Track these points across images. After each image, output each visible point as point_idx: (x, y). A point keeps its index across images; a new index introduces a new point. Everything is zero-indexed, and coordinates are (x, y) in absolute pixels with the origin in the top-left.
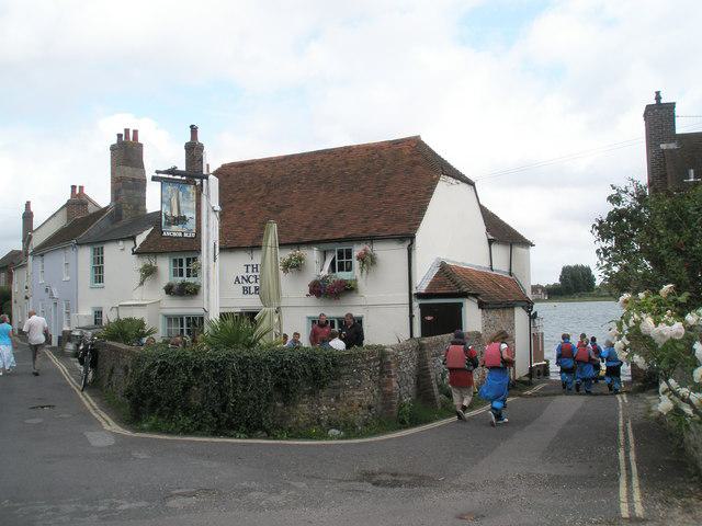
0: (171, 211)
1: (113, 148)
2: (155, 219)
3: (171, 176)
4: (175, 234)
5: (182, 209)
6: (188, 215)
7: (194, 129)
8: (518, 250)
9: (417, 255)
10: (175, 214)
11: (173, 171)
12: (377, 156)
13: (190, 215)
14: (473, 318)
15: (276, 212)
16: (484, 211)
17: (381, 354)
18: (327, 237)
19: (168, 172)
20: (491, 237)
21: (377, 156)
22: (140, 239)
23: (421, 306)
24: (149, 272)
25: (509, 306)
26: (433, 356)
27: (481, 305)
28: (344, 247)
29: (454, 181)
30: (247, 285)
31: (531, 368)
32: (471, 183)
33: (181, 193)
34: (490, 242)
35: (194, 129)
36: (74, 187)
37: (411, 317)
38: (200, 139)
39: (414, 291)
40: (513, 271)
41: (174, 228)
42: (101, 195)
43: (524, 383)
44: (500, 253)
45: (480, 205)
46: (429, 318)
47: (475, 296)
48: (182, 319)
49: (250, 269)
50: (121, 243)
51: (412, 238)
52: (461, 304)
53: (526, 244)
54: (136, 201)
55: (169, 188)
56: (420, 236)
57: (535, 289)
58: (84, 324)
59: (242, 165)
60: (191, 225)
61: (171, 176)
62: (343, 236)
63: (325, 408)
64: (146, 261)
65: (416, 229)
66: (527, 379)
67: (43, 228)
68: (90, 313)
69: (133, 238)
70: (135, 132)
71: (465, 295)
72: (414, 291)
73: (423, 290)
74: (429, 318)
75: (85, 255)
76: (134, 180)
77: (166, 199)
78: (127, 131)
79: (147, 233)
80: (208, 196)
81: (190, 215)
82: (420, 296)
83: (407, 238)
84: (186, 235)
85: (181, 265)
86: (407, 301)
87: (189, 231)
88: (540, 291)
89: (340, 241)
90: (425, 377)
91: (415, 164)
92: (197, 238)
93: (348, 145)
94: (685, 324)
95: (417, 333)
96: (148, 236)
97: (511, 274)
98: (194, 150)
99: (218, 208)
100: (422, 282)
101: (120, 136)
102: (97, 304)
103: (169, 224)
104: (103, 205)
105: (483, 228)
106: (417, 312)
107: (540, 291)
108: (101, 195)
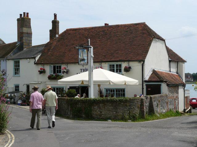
1: (18, 20)
7: (55, 16)
8: (180, 64)
10: (82, 58)
12: (129, 29)
13: (86, 58)
15: (23, 18)
17: (131, 101)
18: (112, 60)
20: (170, 59)
21: (129, 29)
22: (37, 59)
23: (146, 85)
24: (42, 72)
27: (168, 85)
28: (119, 63)
29: (158, 40)
32: (163, 40)
34: (170, 61)
35: (55, 16)
37: (143, 88)
38: (58, 19)
41: (82, 62)
43: (182, 113)
45: (166, 47)
46: (149, 89)
47: (166, 82)
48: (114, 90)
50: (28, 59)
51: (144, 61)
52: (160, 85)
53: (184, 61)
54: (28, 42)
56: (146, 60)
57: (187, 75)
58: (11, 90)
60: (86, 61)
62: (118, 60)
64: (40, 67)
65: (145, 58)
66: (183, 112)
68: (13, 86)
69: (35, 58)
70: (27, 13)
71: (162, 81)
72: (144, 80)
74: (149, 89)
80: (90, 52)
81: (86, 58)
82: (146, 81)
83: (142, 60)
85: (57, 71)
86: (142, 83)
88: (189, 76)
89: (117, 61)
90: (152, 107)
91: (143, 33)
93: (117, 24)
94: (11, 95)
99: (93, 56)
100: (147, 78)
101: (21, 15)
102: (17, 83)
103: (81, 61)
105: (168, 57)
106: (145, 87)
107: (189, 76)
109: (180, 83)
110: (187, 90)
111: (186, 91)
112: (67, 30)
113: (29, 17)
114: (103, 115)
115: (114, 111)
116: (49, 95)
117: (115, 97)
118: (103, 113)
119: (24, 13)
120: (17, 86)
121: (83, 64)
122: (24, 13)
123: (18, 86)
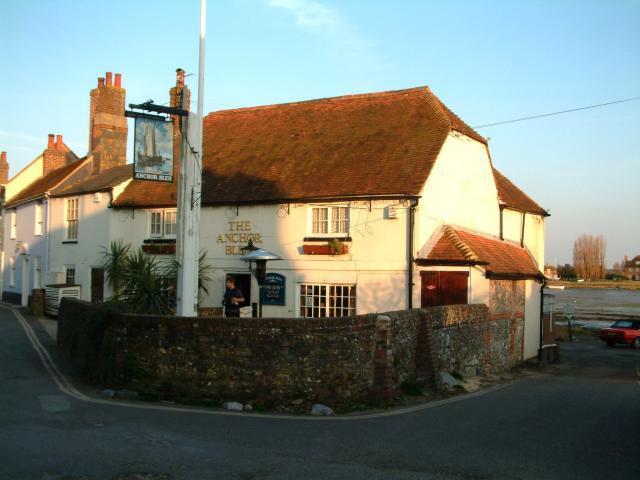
0: (146, 149)
2: (130, 171)
3: (146, 112)
4: (149, 177)
5: (157, 149)
6: (165, 156)
9: (458, 223)
10: (150, 154)
11: (149, 106)
14: (478, 285)
16: (497, 175)
19: (142, 107)
20: (502, 203)
22: (118, 190)
23: (423, 274)
25: (517, 276)
26: (434, 328)
27: (488, 275)
30: (232, 244)
31: (540, 351)
33: (157, 131)
34: (502, 207)
36: (51, 136)
37: (410, 285)
39: (415, 256)
40: (504, 237)
41: (149, 169)
42: (80, 147)
44: (512, 217)
46: (431, 287)
49: (235, 227)
52: (467, 274)
55: (143, 124)
59: (231, 113)
60: (168, 167)
61: (146, 112)
63: (309, 380)
67: (17, 179)
69: (109, 190)
70: (118, 77)
73: (425, 257)
74: (431, 287)
75: (38, 209)
76: (114, 128)
77: (139, 137)
78: (109, 75)
79: (125, 184)
82: (422, 262)
83: (413, 197)
84: (161, 178)
87: (166, 174)
92: (175, 181)
95: (417, 304)
96: (127, 189)
97: (522, 245)
98: (179, 94)
100: (423, 244)
101: (101, 80)
104: (81, 156)
105: (494, 191)
106: (418, 282)
108: (80, 147)
109: (532, 272)
110: (549, 296)
111: (546, 300)
112: (203, 146)
113: (123, 86)
114: (210, 379)
115: (257, 368)
116: (486, 302)
117: (224, 315)
118: (211, 373)
119: (107, 74)
120: (339, 288)
121: (155, 177)
122: (107, 74)
123: (74, 270)
